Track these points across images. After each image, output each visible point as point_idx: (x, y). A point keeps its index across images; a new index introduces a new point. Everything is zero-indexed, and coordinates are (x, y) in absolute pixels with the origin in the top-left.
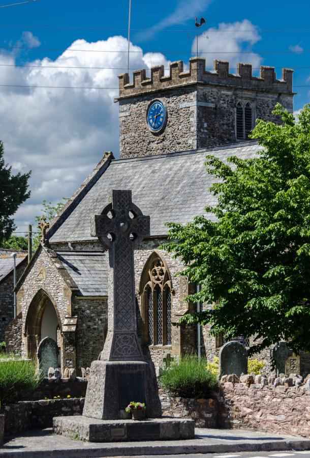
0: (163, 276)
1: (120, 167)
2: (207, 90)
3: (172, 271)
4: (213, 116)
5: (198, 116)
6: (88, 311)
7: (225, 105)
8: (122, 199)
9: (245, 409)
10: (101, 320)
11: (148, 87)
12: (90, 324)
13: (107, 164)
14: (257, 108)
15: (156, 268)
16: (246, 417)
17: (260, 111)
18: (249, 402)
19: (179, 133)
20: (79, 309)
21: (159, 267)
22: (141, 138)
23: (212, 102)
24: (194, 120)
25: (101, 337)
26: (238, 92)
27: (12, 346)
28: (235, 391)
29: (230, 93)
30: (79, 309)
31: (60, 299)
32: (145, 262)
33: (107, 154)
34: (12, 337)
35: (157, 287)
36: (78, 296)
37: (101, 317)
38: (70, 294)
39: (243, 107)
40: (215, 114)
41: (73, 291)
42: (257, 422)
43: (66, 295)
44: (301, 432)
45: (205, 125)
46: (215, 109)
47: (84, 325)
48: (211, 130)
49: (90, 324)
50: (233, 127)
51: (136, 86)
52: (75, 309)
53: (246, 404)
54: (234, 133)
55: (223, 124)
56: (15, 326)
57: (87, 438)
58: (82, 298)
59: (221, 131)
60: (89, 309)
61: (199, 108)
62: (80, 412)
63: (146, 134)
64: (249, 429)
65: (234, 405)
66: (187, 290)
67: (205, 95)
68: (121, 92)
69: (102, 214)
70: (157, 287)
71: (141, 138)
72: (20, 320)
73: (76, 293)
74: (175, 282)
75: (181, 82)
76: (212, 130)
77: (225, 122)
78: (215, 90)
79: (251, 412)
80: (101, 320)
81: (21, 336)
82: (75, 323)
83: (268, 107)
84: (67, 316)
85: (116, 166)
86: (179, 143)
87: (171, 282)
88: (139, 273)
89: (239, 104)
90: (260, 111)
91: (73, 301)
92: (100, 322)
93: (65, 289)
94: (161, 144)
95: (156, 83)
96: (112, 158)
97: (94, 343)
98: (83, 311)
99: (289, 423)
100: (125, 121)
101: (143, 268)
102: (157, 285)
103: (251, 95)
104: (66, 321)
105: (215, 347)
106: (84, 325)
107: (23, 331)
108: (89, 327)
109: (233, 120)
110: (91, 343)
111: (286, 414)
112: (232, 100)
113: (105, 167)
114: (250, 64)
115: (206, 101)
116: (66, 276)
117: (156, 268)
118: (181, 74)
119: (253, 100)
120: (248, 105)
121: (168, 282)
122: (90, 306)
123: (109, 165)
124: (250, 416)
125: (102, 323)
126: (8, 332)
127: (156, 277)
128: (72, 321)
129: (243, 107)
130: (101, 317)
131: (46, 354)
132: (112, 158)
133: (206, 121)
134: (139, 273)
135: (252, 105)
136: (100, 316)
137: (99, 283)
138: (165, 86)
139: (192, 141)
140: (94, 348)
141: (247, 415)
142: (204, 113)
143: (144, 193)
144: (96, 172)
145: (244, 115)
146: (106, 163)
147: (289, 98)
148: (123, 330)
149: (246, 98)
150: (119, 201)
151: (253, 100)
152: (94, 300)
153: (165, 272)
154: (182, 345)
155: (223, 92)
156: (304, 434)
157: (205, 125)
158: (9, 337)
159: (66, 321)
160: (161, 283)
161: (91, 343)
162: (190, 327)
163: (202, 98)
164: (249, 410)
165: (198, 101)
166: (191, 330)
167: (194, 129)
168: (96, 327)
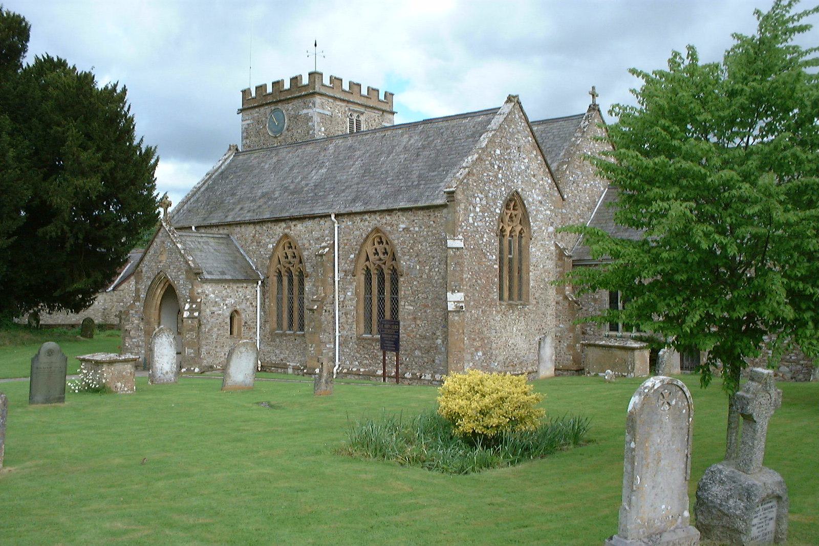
3: (305, 253)
10: (226, 305)
12: (214, 309)
31: (181, 282)
49: (214, 309)
74: (308, 265)
80: (226, 305)
97: (219, 330)
106: (208, 310)
136: (225, 300)
161: (216, 329)
168: (220, 312)
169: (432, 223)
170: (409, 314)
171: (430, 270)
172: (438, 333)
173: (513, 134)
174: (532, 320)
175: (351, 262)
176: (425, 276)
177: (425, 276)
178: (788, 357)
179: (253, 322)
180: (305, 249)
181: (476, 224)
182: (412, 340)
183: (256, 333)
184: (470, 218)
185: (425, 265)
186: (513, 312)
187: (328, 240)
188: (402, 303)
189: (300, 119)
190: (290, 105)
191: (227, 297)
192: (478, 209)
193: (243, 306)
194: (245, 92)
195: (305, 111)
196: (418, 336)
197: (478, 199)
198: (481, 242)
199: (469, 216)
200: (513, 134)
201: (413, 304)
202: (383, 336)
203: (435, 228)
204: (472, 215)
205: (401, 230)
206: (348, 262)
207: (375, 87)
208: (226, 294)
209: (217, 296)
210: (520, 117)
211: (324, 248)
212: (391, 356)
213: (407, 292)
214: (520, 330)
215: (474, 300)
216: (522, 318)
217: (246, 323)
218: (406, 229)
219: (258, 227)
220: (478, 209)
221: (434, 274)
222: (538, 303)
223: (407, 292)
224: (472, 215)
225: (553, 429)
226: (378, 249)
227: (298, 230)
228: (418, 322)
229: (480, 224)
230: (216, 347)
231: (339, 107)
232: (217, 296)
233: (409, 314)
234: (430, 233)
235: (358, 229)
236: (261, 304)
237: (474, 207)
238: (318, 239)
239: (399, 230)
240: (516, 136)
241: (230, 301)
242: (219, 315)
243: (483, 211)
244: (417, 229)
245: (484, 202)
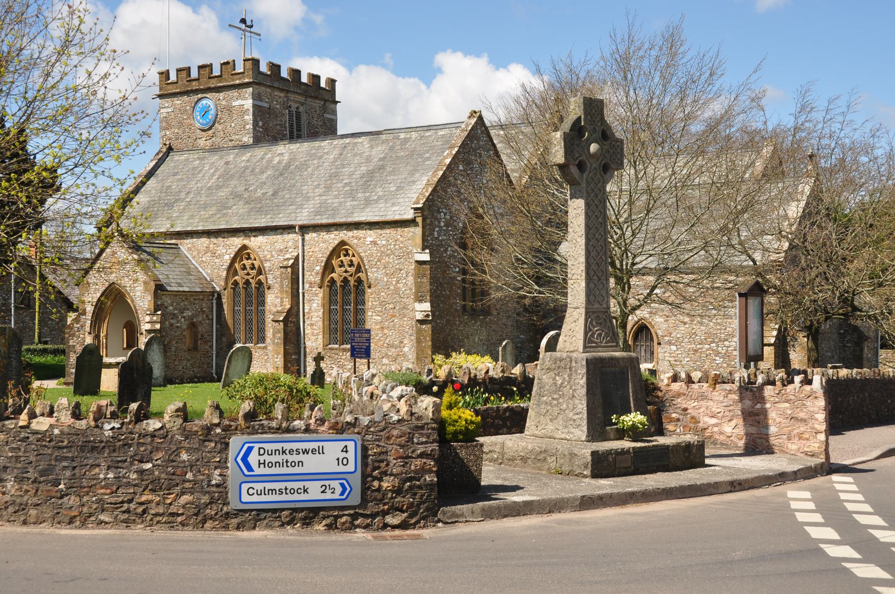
0: (255, 271)
1: (183, 158)
2: (262, 89)
3: (267, 265)
4: (267, 116)
5: (254, 114)
6: (171, 308)
7: (278, 106)
8: (594, 111)
9: (707, 419)
10: (184, 317)
11: (194, 83)
12: (172, 321)
13: (166, 155)
14: (306, 112)
15: (245, 262)
16: (709, 431)
17: (309, 115)
18: (714, 409)
19: (229, 129)
20: (162, 305)
21: (249, 261)
22: (187, 134)
23: (266, 102)
24: (249, 118)
25: (184, 336)
26: (289, 95)
27: (74, 346)
28: (690, 394)
29: (282, 95)
30: (162, 305)
31: (138, 294)
32: (232, 256)
33: (165, 144)
34: (73, 335)
35: (247, 283)
36: (161, 290)
37: (184, 315)
38: (153, 288)
39: (293, 109)
40: (269, 114)
41: (156, 285)
42: (727, 437)
43: (146, 290)
44: (806, 449)
45: (261, 123)
46: (269, 109)
47: (167, 323)
48: (266, 130)
49: (172, 321)
50: (286, 128)
51: (180, 83)
52: (158, 305)
53: (708, 412)
54: (286, 134)
55: (277, 125)
56: (77, 324)
57: (587, 472)
58: (165, 293)
59: (275, 131)
60: (172, 305)
61: (254, 106)
62: (521, 430)
63: (192, 131)
64: (713, 446)
65: (687, 414)
66: (290, 285)
67: (259, 94)
68: (161, 89)
69: (571, 130)
70: (247, 283)
71: (187, 134)
72: (84, 317)
73: (159, 289)
74: (270, 277)
75: (233, 80)
76: (267, 129)
77: (279, 122)
78: (268, 90)
79: (718, 423)
80: (184, 317)
81: (84, 334)
82: (159, 320)
83: (316, 111)
84: (148, 313)
85: (176, 158)
86: (231, 141)
87: (266, 277)
88: (223, 267)
89: (290, 107)
90: (309, 115)
91: (156, 296)
92: (183, 320)
93: (145, 283)
94: (210, 141)
95: (202, 80)
96: (170, 149)
97: (177, 342)
98: (166, 308)
99: (785, 437)
100: (166, 117)
101: (229, 262)
102: (247, 280)
103: (301, 99)
104: (148, 319)
105: (321, 346)
106: (167, 323)
107: (88, 329)
108: (172, 325)
109: (286, 122)
110: (174, 342)
111: (778, 425)
112: (284, 102)
113: (164, 158)
114: (299, 69)
115: (261, 100)
116: (146, 270)
117: (245, 262)
118: (234, 72)
119: (302, 104)
120: (297, 108)
121: (261, 277)
122: (173, 302)
123: (168, 156)
124: (716, 429)
125: (185, 320)
126: (68, 331)
127: (245, 272)
128: (155, 318)
129: (293, 109)
130: (184, 315)
131: (152, 354)
132: (170, 149)
133: (261, 120)
134: (223, 267)
135: (301, 109)
136: (183, 313)
137: (180, 277)
138: (213, 84)
139: (248, 139)
140: (177, 348)
141: (710, 428)
142: (259, 112)
143: (220, 184)
144: (154, 162)
145: (294, 118)
146: (164, 154)
147: (333, 106)
148: (595, 306)
149: (296, 102)
150: (589, 114)
151: (302, 104)
152: (176, 295)
153: (256, 266)
154: (285, 344)
155: (275, 93)
156: (811, 452)
157: (261, 123)
158: (70, 336)
159: (148, 319)
160: (253, 278)
161: (174, 342)
162: (292, 325)
163: (256, 97)
164: (713, 421)
165: (253, 99)
166: (294, 328)
167: (250, 126)
168: (179, 325)
169: (399, 237)
170: (376, 324)
171: (398, 282)
172: (406, 341)
173: (475, 150)
174: (494, 331)
175: (317, 274)
176: (392, 288)
177: (392, 288)
178: (733, 363)
179: (209, 335)
180: (266, 260)
181: (440, 238)
182: (379, 349)
183: (211, 346)
184: (436, 233)
185: (392, 276)
186: (475, 323)
187: (292, 252)
188: (370, 314)
189: (234, 111)
190: (221, 94)
191: (185, 309)
192: (442, 224)
193: (200, 319)
194: (165, 75)
195: (239, 102)
196: (385, 345)
197: (442, 214)
198: (445, 255)
199: (434, 231)
200: (475, 150)
201: (381, 314)
202: (353, 344)
203: (402, 242)
204: (437, 229)
205: (369, 243)
206: (313, 273)
207: (315, 73)
208: (183, 307)
209: (175, 309)
210: (482, 132)
211: (288, 259)
212: (361, 363)
213: (375, 303)
214: (481, 340)
215: (439, 311)
216: (484, 329)
217: (202, 336)
218: (374, 243)
219: (214, 240)
220: (442, 224)
221: (402, 285)
222: (499, 314)
223: (375, 303)
224: (437, 229)
225: (531, 103)
226: (344, 261)
227: (255, 242)
228: (386, 331)
229: (444, 238)
230: (175, 360)
231: (276, 97)
232: (175, 309)
233: (376, 324)
234: (397, 247)
235: (324, 242)
236: (217, 316)
237: (439, 222)
238: (281, 251)
239: (367, 243)
240: (478, 151)
241: (188, 313)
242: (178, 327)
243: (447, 225)
244: (384, 242)
245: (448, 217)
